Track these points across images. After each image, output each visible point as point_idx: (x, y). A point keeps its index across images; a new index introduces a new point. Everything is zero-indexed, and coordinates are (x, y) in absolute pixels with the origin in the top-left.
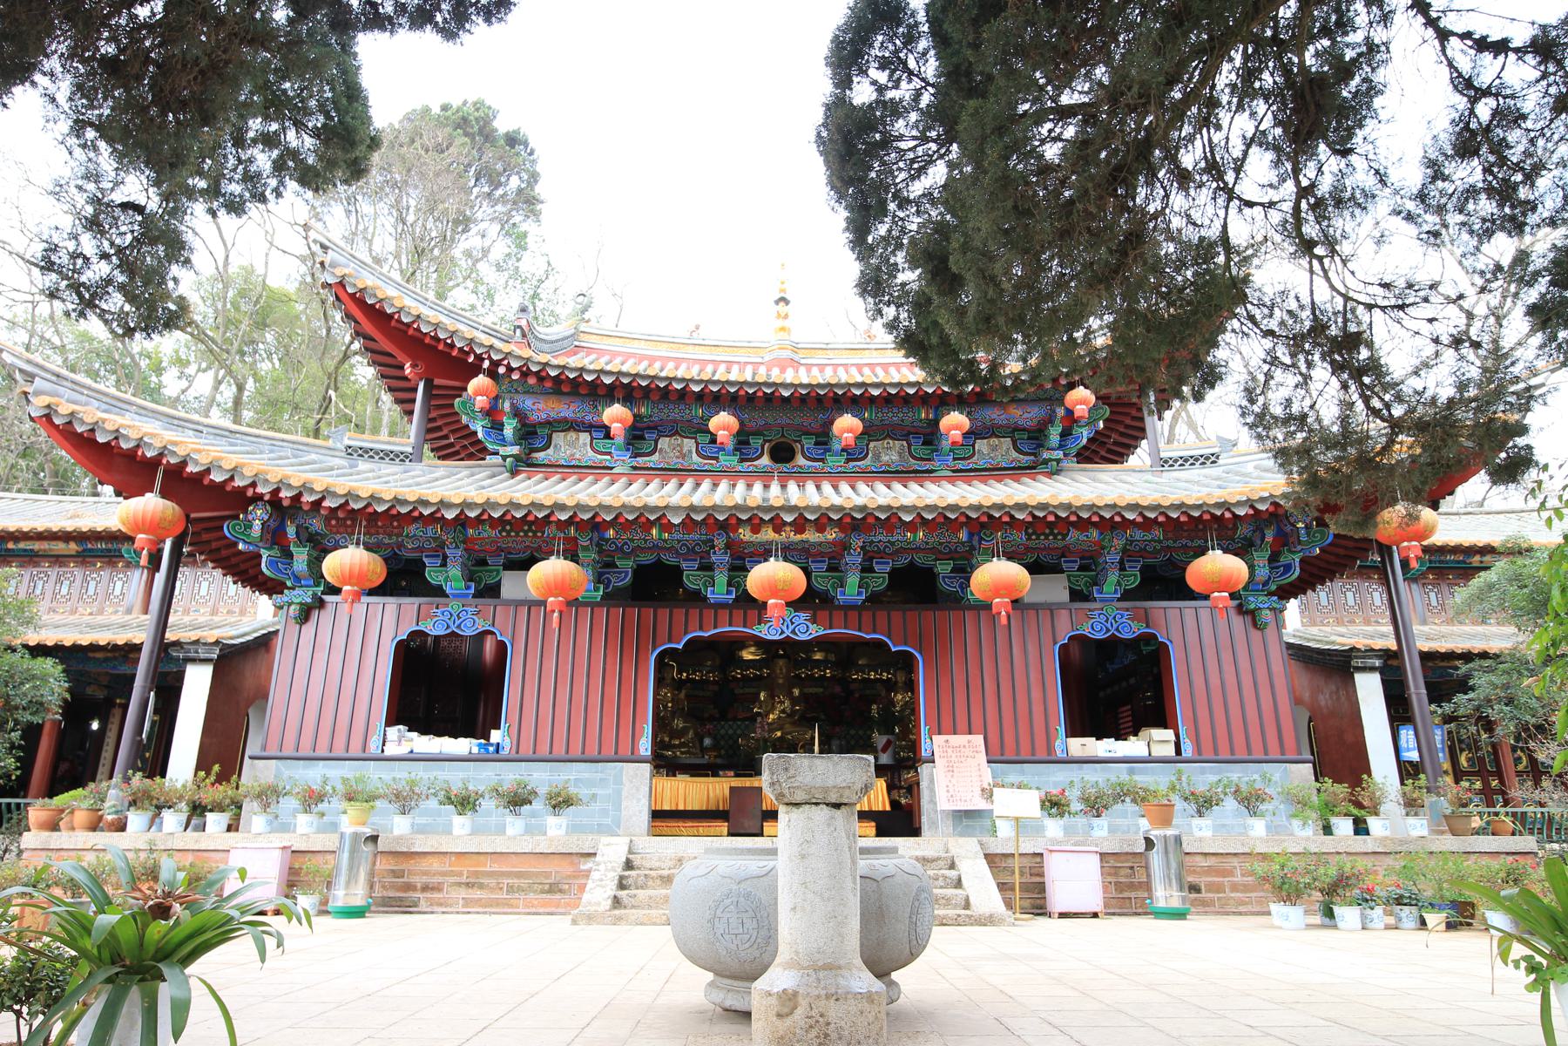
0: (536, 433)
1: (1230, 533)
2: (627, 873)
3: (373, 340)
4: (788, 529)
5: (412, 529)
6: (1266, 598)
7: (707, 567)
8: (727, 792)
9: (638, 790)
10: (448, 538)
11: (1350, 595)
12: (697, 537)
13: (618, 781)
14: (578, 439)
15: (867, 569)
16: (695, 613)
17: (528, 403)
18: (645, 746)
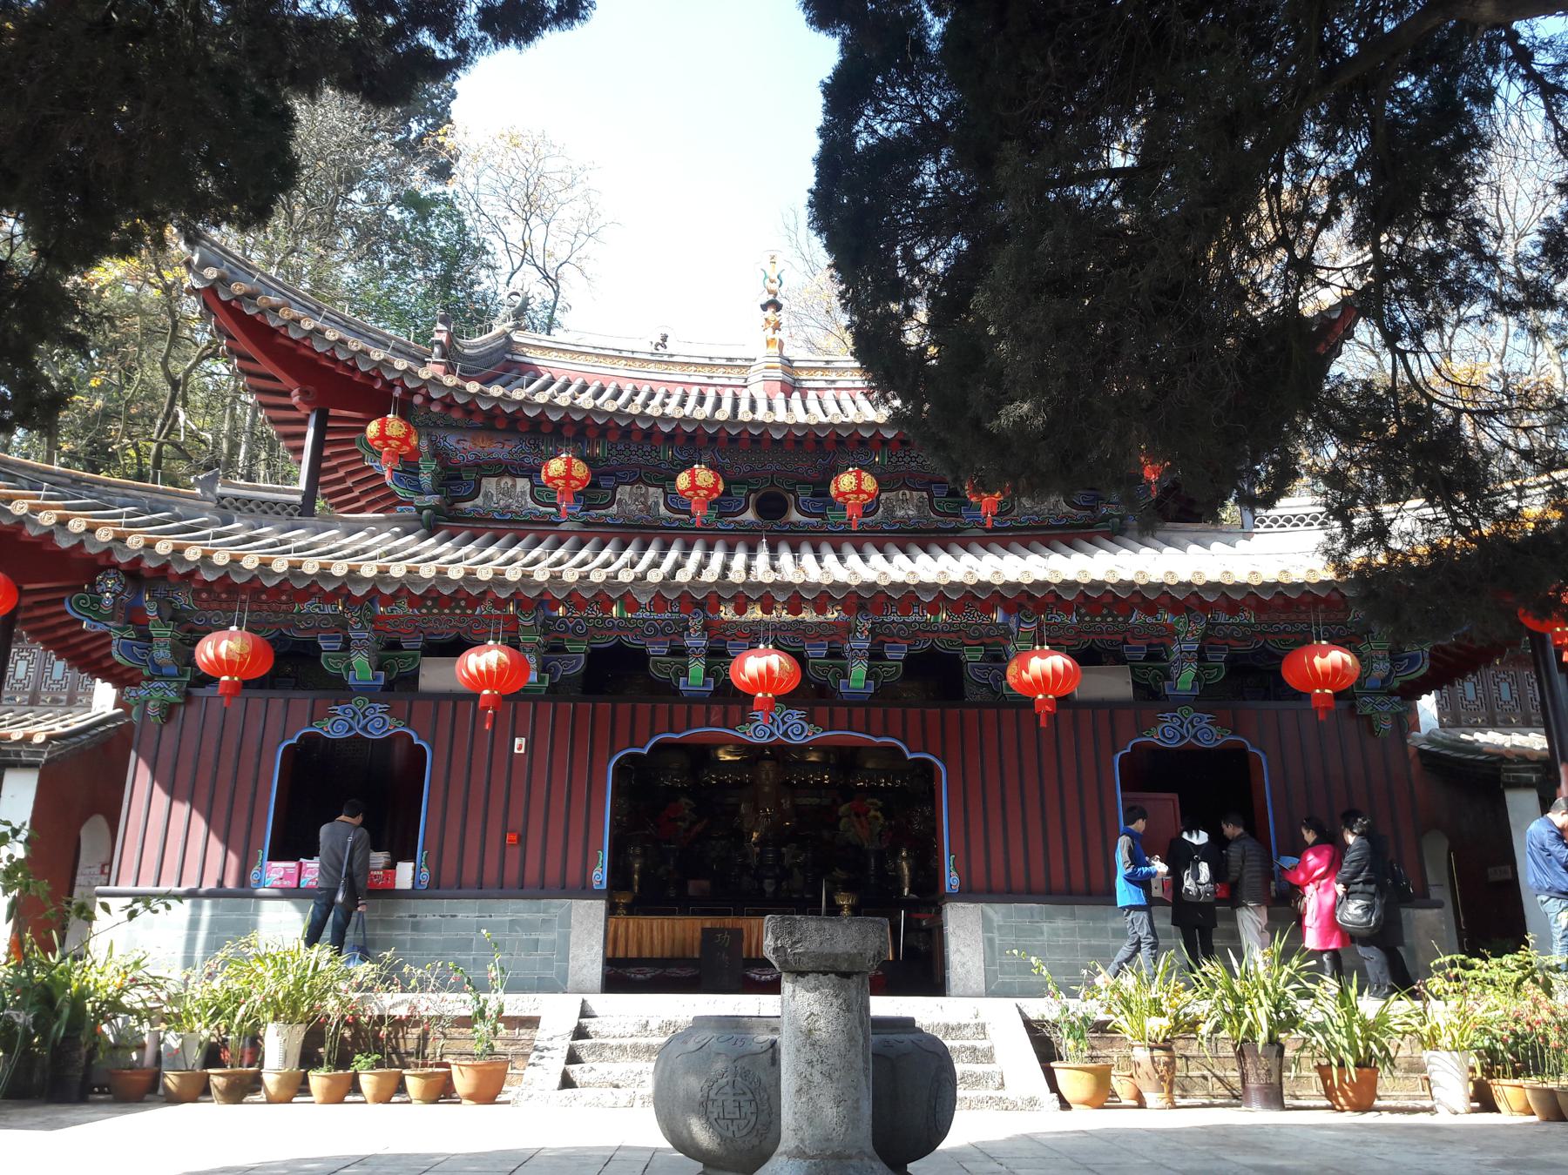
0: (460, 478)
1: (1340, 615)
2: (579, 1042)
3: (253, 360)
4: (779, 606)
5: (308, 607)
6: (1385, 699)
7: (679, 652)
8: (698, 934)
9: (590, 933)
10: (352, 617)
11: (1504, 687)
12: (666, 615)
13: (565, 923)
14: (514, 486)
15: (875, 656)
16: (663, 707)
17: (451, 441)
18: (600, 876)
